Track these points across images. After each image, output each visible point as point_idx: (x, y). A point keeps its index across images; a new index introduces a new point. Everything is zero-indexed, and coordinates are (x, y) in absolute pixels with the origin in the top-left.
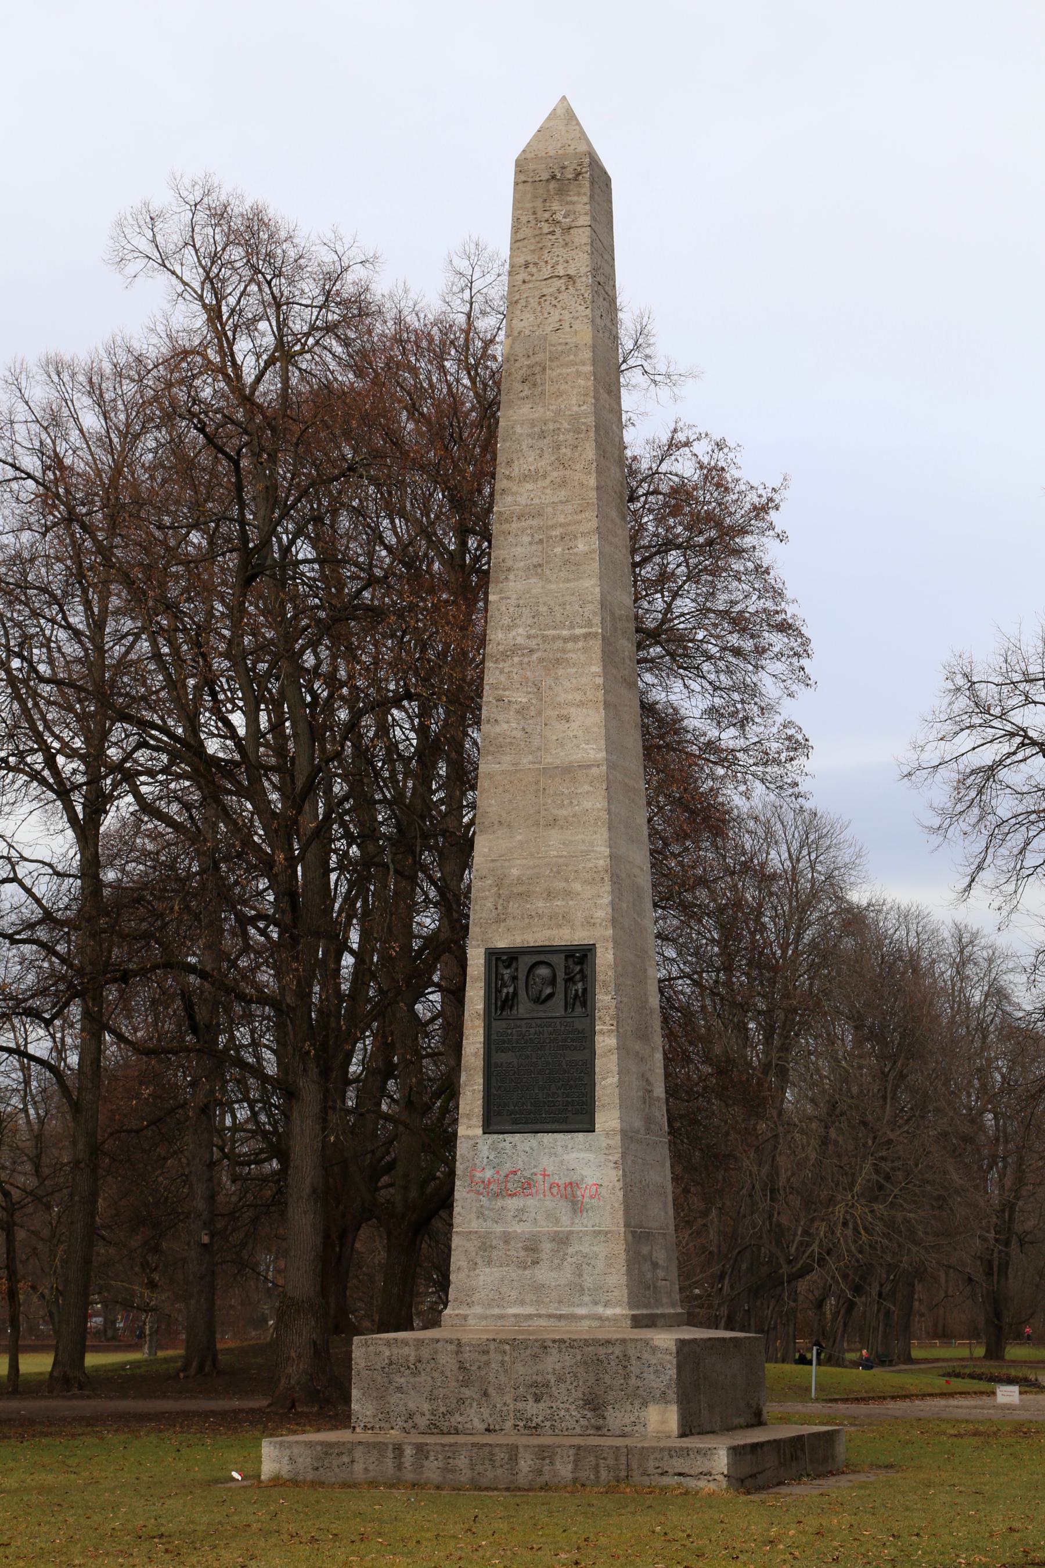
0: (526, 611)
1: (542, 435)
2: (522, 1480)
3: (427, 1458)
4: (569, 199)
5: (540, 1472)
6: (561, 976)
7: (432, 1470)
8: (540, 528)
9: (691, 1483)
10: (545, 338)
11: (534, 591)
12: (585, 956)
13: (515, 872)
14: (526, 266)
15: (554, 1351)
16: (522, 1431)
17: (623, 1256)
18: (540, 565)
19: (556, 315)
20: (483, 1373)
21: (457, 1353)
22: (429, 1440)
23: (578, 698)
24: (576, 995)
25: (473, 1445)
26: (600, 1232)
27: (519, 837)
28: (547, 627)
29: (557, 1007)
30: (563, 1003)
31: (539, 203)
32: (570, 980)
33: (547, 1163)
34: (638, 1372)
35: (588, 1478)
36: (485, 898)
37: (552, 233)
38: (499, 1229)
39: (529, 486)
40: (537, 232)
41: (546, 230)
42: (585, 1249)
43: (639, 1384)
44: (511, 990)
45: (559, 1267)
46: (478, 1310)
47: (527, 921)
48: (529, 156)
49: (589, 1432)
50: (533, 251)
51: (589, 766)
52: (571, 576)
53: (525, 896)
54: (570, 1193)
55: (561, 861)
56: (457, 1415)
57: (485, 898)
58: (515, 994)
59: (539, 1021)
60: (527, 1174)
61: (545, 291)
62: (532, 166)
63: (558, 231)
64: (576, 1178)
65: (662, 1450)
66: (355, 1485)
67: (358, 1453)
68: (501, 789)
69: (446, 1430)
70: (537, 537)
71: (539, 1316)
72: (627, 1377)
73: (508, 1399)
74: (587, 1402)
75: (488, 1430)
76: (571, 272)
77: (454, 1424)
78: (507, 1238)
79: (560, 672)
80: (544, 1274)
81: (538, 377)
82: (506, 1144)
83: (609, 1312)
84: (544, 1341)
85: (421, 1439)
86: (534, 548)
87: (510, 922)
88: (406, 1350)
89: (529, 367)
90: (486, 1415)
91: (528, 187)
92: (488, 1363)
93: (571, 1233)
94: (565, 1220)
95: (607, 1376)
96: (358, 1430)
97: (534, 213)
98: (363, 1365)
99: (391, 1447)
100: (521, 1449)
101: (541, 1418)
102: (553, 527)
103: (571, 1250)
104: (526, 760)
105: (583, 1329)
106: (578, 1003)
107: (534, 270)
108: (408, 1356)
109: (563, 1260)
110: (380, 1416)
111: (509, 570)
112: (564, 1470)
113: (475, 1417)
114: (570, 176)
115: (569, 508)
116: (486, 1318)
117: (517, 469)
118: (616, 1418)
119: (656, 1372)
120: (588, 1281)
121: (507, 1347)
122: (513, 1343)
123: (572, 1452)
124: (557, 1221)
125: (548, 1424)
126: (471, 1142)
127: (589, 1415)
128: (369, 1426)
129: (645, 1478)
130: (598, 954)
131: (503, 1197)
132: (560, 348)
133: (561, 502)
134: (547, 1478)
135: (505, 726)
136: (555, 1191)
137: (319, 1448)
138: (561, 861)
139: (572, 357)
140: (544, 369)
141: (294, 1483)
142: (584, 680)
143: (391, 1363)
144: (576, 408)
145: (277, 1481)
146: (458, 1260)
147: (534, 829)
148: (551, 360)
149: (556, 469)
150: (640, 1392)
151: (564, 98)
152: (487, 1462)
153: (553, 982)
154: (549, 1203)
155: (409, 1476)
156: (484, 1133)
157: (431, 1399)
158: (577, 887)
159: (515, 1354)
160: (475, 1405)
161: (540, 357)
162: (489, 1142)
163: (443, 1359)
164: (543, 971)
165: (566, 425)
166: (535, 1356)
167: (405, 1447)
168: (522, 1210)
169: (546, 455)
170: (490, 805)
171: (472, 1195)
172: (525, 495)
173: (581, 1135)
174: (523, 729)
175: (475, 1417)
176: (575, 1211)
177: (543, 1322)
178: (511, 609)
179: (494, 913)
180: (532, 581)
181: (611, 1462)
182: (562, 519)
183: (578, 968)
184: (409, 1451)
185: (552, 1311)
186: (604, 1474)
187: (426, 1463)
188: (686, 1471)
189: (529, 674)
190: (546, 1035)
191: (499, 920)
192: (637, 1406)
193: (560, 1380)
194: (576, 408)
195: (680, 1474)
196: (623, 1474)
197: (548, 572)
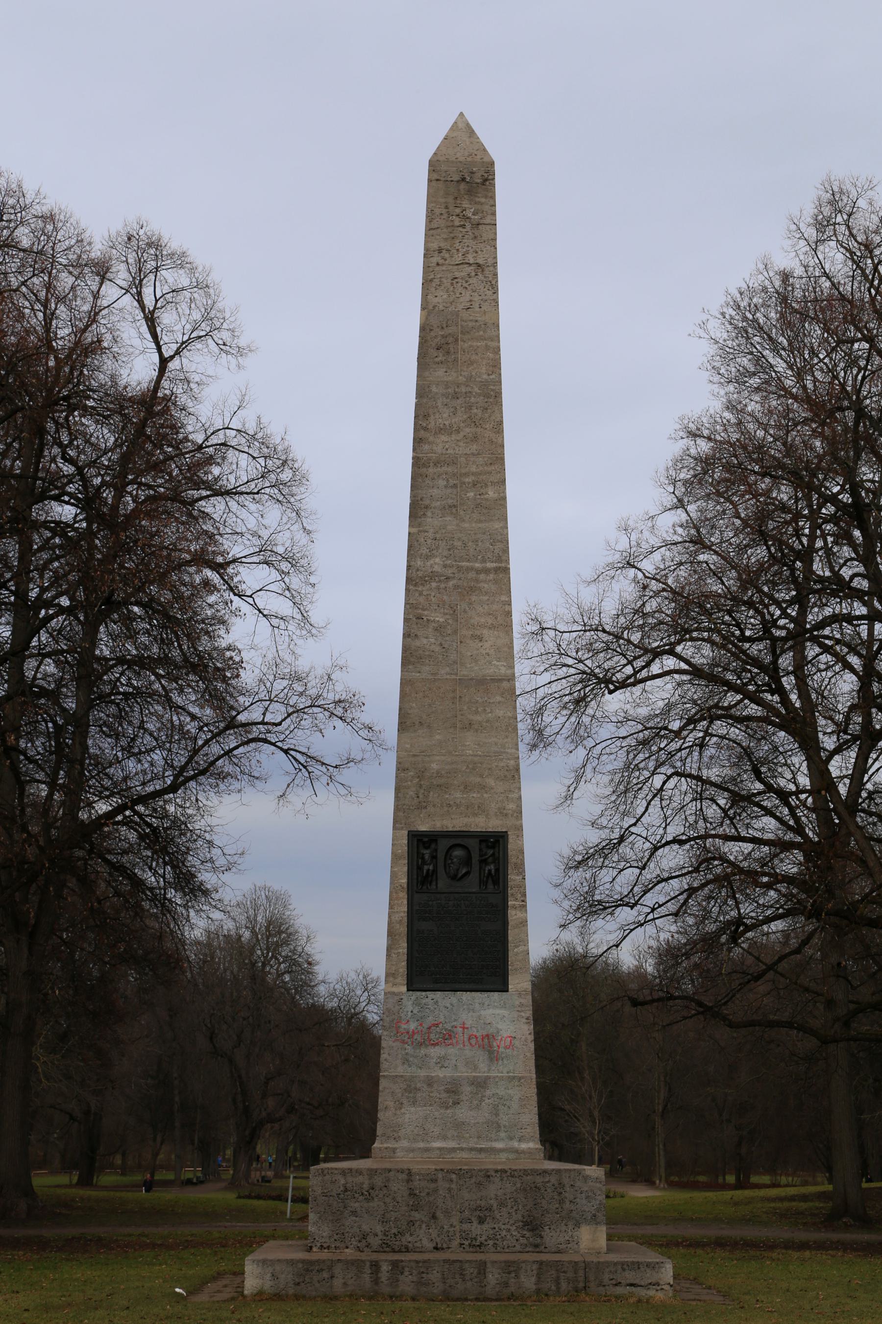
0: (442, 544)
2: (489, 1291)
3: (402, 1273)
4: (477, 199)
5: (506, 1284)
7: (407, 1283)
8: (454, 475)
9: (642, 1292)
10: (457, 314)
11: (449, 527)
13: (434, 766)
15: (497, 1180)
16: (467, 1249)
17: (535, 1098)
18: (455, 506)
19: (467, 296)
20: (431, 1199)
21: (408, 1181)
22: (383, 1256)
23: (490, 621)
25: (445, 1261)
26: (514, 1077)
27: (438, 737)
28: (462, 559)
29: (472, 884)
31: (450, 200)
32: (483, 862)
33: (467, 1018)
34: (572, 1197)
35: (550, 1289)
36: (408, 788)
37: (463, 226)
38: (423, 1073)
39: (444, 438)
41: (457, 223)
42: (501, 1092)
43: (573, 1208)
44: (431, 868)
45: (478, 1107)
46: (405, 1143)
47: (446, 809)
48: (442, 159)
49: (527, 1249)
50: (446, 240)
51: (501, 680)
52: (483, 518)
53: (443, 788)
54: (487, 1043)
55: (476, 759)
56: (407, 1235)
57: (408, 788)
58: (435, 871)
60: (448, 1026)
61: (457, 274)
62: (444, 167)
63: (468, 226)
64: (492, 1031)
65: (615, 1264)
66: (335, 1298)
67: (338, 1270)
68: (421, 694)
69: (397, 1249)
70: (452, 482)
71: (462, 1149)
72: (561, 1202)
73: (455, 1221)
74: (526, 1224)
75: (436, 1248)
76: (480, 261)
77: (405, 1243)
78: (430, 1082)
79: (474, 598)
80: (463, 1113)
81: (451, 346)
82: (429, 1000)
83: (524, 1146)
84: (487, 1170)
85: (374, 1257)
86: (449, 491)
87: (431, 809)
88: (360, 1179)
89: (443, 336)
90: (434, 1235)
91: (441, 185)
92: (436, 1190)
93: (488, 1078)
94: (483, 1066)
95: (544, 1202)
96: (314, 1249)
97: (447, 207)
98: (320, 1192)
99: (368, 1264)
100: (489, 1265)
101: (484, 1238)
102: (466, 475)
103: (488, 1093)
104: (444, 671)
105: (502, 1161)
106: (490, 881)
107: (447, 256)
108: (363, 1183)
109: (481, 1101)
110: (336, 1237)
111: (426, 507)
112: (529, 1282)
113: (423, 1237)
114: (479, 181)
115: (480, 460)
116: (413, 1150)
118: (552, 1237)
119: (587, 1197)
120: (504, 1120)
121: (454, 1176)
122: (459, 1173)
123: (535, 1267)
124: (476, 1068)
125: (491, 1242)
126: (397, 998)
127: (528, 1234)
128: (325, 1245)
129: (601, 1288)
130: (510, 840)
131: (426, 1046)
132: (471, 324)
133: (473, 454)
134: (512, 1289)
135: (425, 641)
136: (473, 1041)
137: (300, 1265)
138: (476, 759)
139: (481, 333)
140: (457, 340)
141: (278, 1297)
142: (495, 607)
143: (346, 1190)
144: (485, 376)
145: (260, 1296)
146: (385, 1100)
147: (451, 730)
148: (462, 333)
149: (468, 426)
150: (574, 1214)
151: (461, 114)
152: (457, 1276)
154: (468, 1052)
155: (386, 1289)
156: (408, 990)
157: (384, 1221)
158: (491, 782)
159: (461, 1182)
160: (424, 1226)
161: (451, 330)
163: (394, 1186)
164: (458, 853)
165: (476, 390)
166: (479, 1184)
167: (381, 1263)
169: (459, 413)
170: (411, 708)
171: (398, 1044)
172: (441, 446)
173: (496, 994)
174: (441, 644)
175: (423, 1237)
176: (491, 1060)
177: (465, 1155)
178: (429, 541)
179: (416, 801)
180: (448, 519)
181: (570, 1275)
182: (474, 469)
183: (491, 852)
184: (385, 1267)
185: (472, 1145)
186: (564, 1285)
187: (401, 1278)
188: (637, 1282)
189: (445, 597)
192: (570, 1227)
193: (502, 1204)
194: (485, 376)
195: (631, 1285)
196: (581, 1285)
197: (462, 513)
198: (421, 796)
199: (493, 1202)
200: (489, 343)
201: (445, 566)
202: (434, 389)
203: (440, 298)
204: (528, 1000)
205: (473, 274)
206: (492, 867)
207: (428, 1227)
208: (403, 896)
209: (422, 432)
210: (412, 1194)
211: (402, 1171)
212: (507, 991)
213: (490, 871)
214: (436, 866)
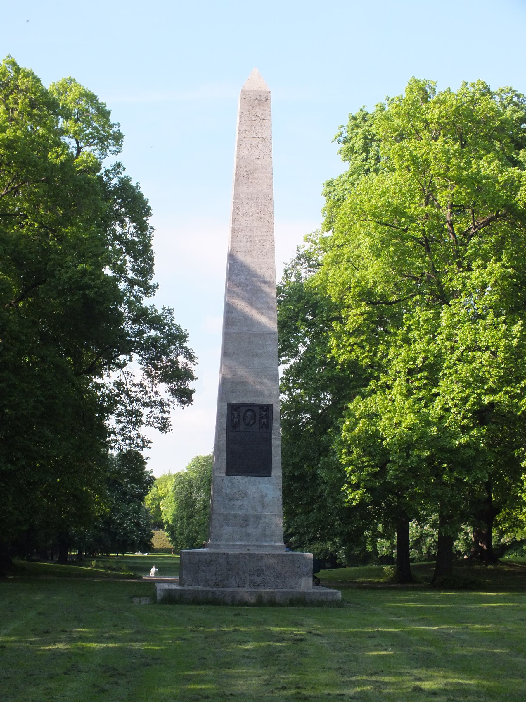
1: (252, 199)
6: (258, 416)
14: (245, 131)
19: (257, 153)
31: (251, 108)
38: (232, 512)
39: (247, 219)
40: (249, 119)
44: (237, 420)
45: (257, 527)
46: (224, 543)
52: (263, 257)
56: (226, 581)
58: (239, 422)
61: (253, 142)
70: (249, 240)
78: (235, 516)
80: (250, 530)
86: (248, 243)
101: (260, 582)
107: (249, 133)
109: (258, 524)
117: (241, 211)
121: (247, 557)
124: (256, 510)
135: (236, 314)
160: (233, 577)
162: (228, 479)
164: (249, 413)
168: (242, 506)
172: (244, 223)
173: (266, 478)
178: (239, 267)
183: (264, 413)
185: (254, 544)
191: (233, 392)
194: (266, 190)
198: (233, 387)
199: (264, 568)
200: (268, 175)
201: (246, 279)
202: (242, 195)
203: (245, 153)
204: (280, 481)
205: (260, 142)
206: (265, 420)
207: (235, 577)
208: (225, 433)
209: (236, 215)
210: (228, 563)
211: (224, 554)
212: (271, 476)
213: (264, 422)
214: (240, 419)
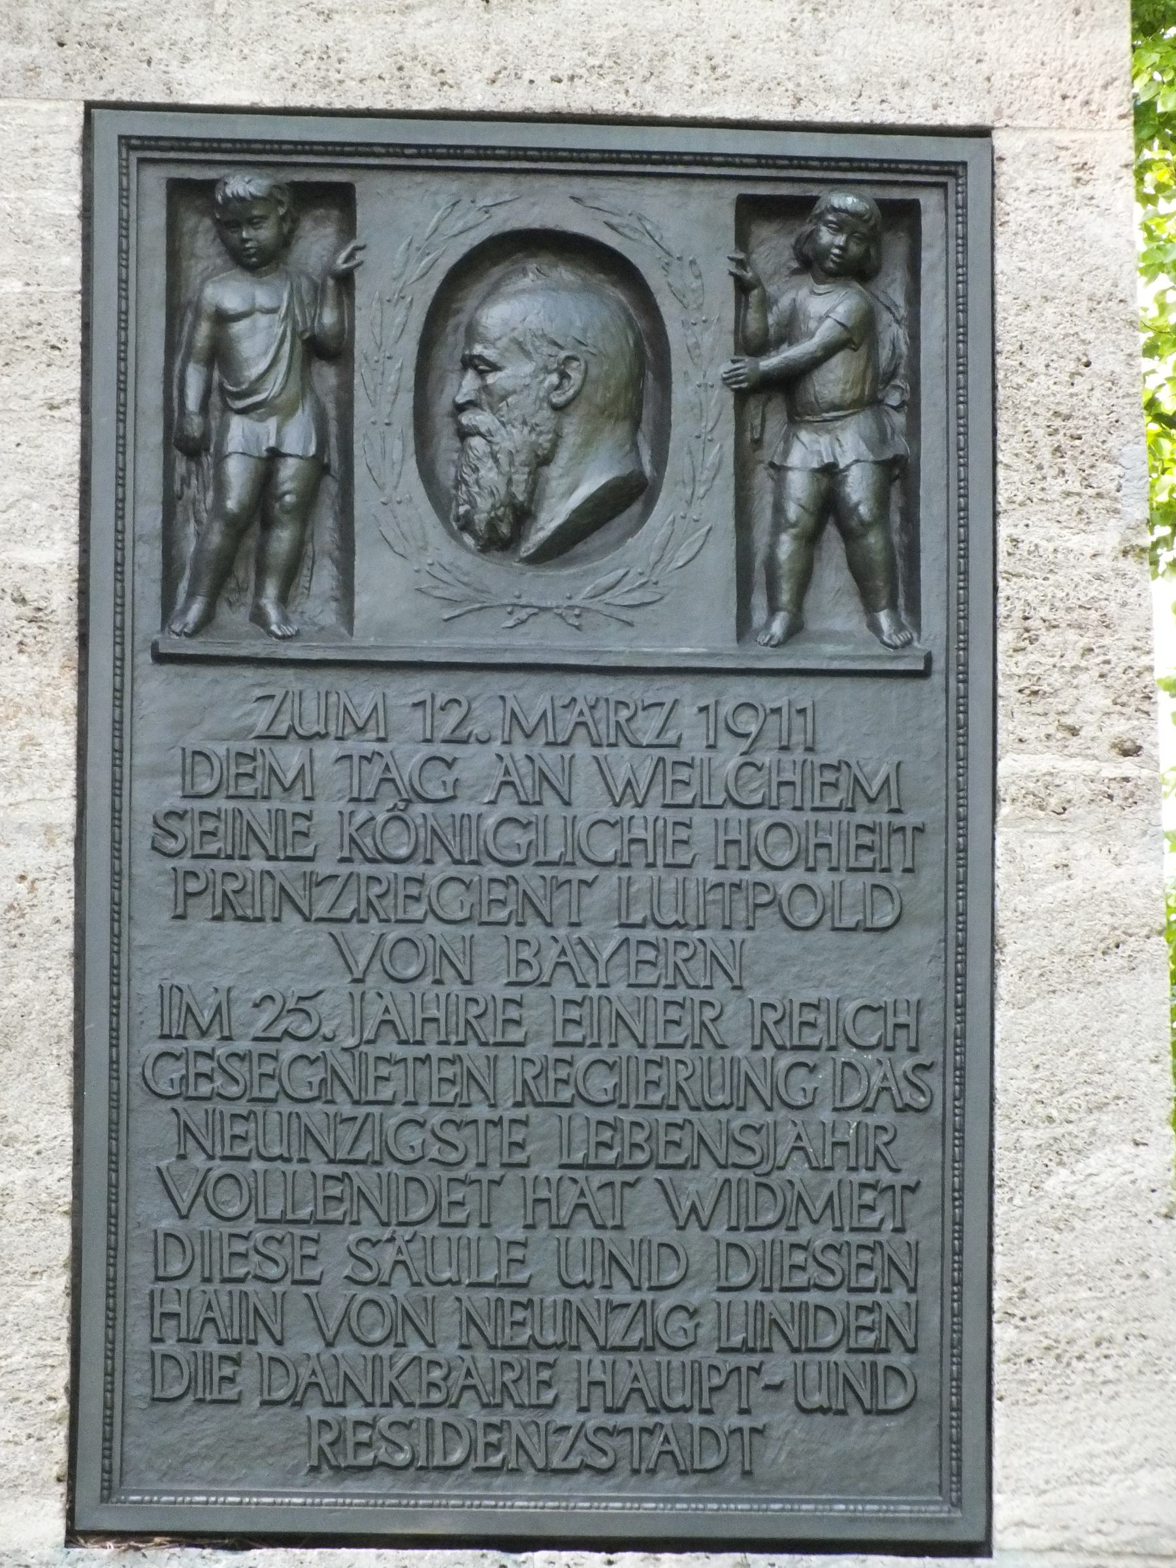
12: (903, 216)
24: (829, 500)
30: (721, 557)
32: (776, 392)
44: (298, 437)
58: (332, 467)
59: (534, 697)
153: (641, 383)
190: (589, 799)
